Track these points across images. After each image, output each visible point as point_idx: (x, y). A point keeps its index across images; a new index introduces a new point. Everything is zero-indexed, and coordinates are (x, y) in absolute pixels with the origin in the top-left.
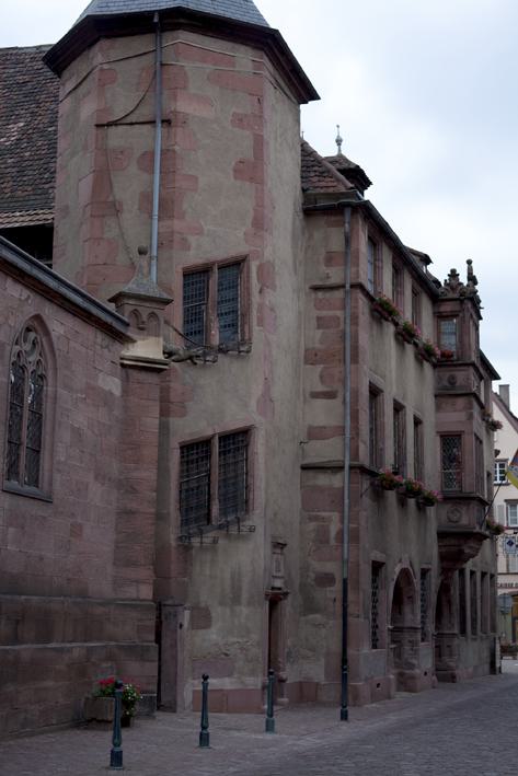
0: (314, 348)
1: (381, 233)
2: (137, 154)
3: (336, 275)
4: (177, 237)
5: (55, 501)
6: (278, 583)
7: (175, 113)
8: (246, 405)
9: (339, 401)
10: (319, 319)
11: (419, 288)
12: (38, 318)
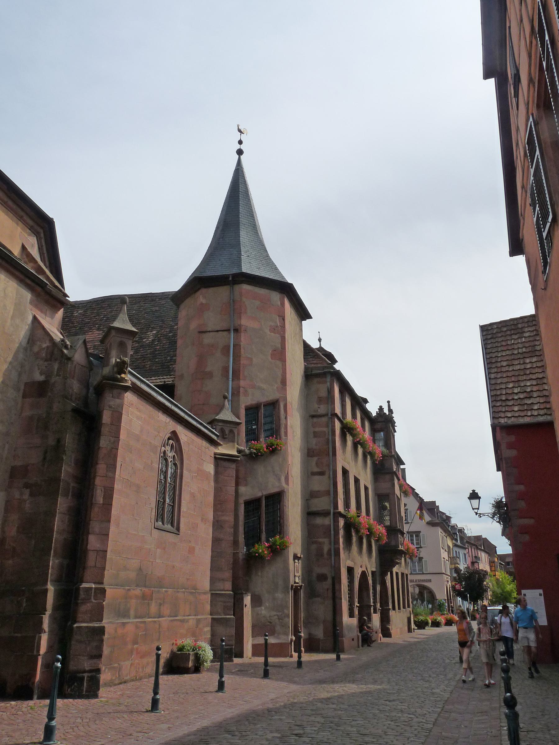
1: (346, 388)
3: (322, 409)
7: (240, 325)
8: (279, 480)
11: (363, 416)
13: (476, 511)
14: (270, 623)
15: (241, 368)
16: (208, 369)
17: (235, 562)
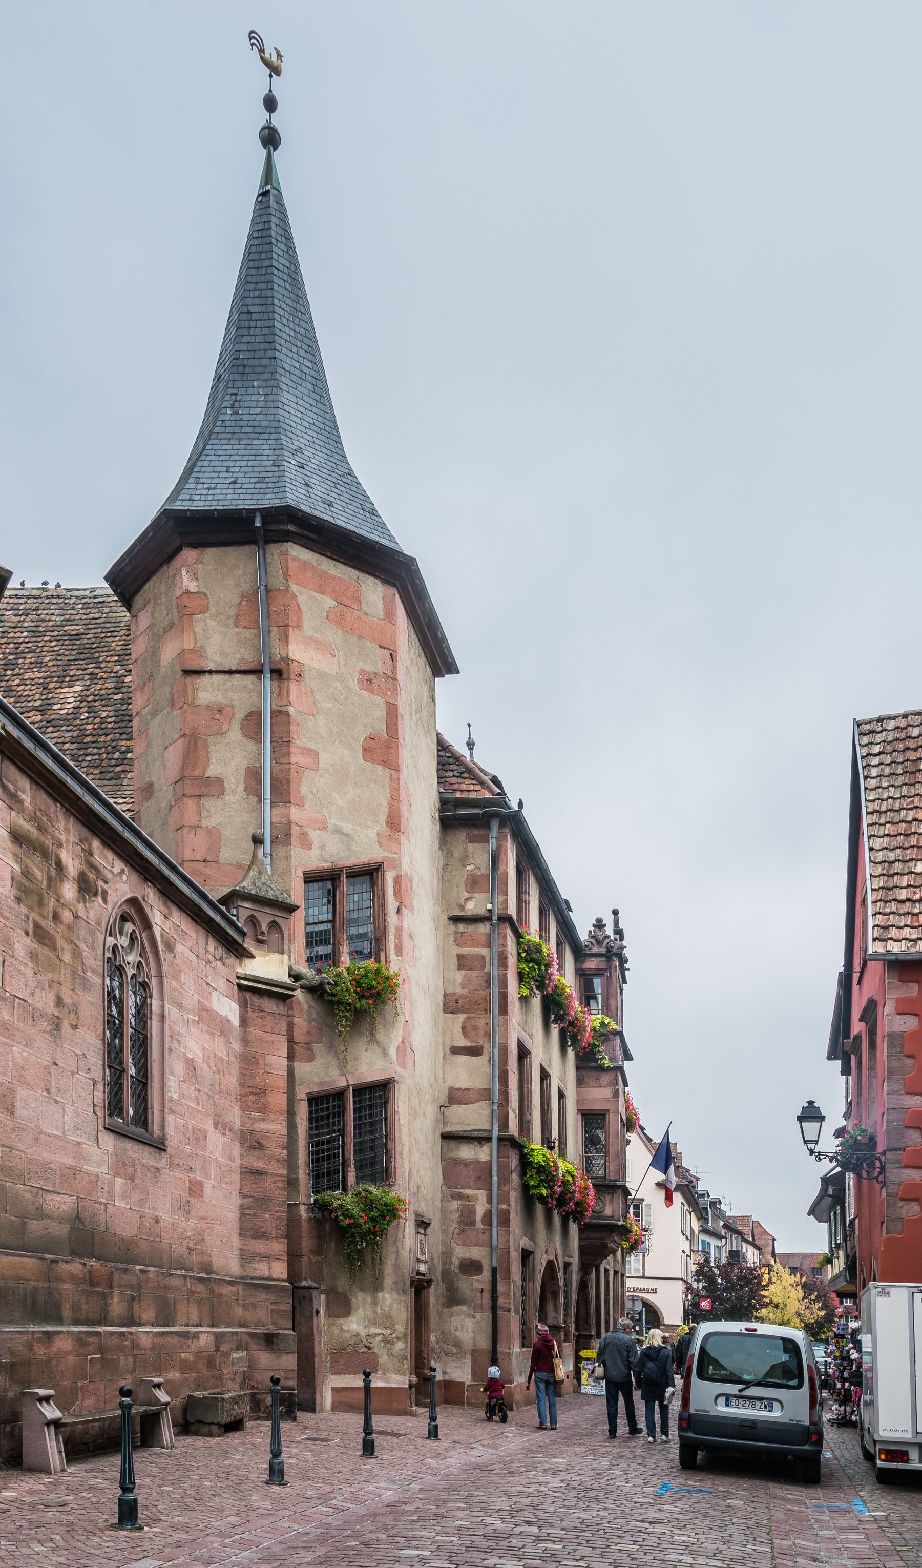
0: (454, 994)
2: (240, 715)
4: (295, 830)
5: (169, 1149)
6: (423, 1268)
7: (287, 660)
9: (485, 1058)
10: (460, 957)
11: (563, 938)
12: (133, 902)
13: (811, 1146)
14: (369, 1348)
15: (293, 773)
16: (212, 771)
17: (292, 1223)
